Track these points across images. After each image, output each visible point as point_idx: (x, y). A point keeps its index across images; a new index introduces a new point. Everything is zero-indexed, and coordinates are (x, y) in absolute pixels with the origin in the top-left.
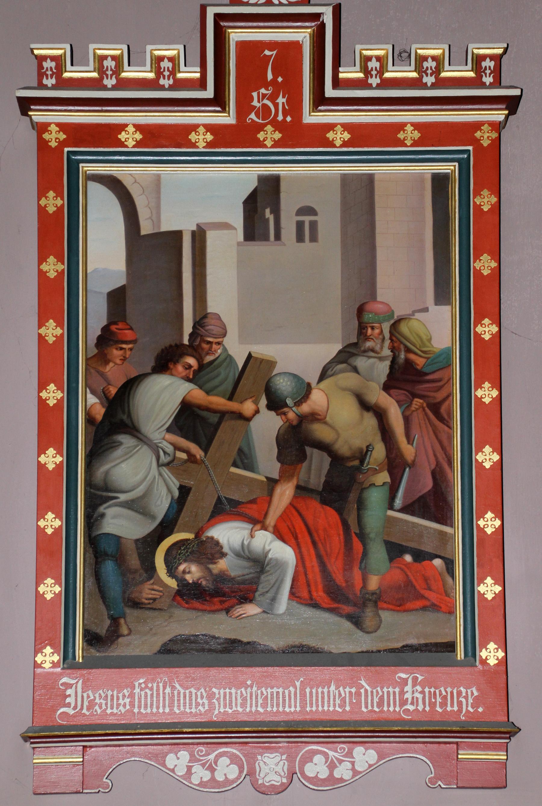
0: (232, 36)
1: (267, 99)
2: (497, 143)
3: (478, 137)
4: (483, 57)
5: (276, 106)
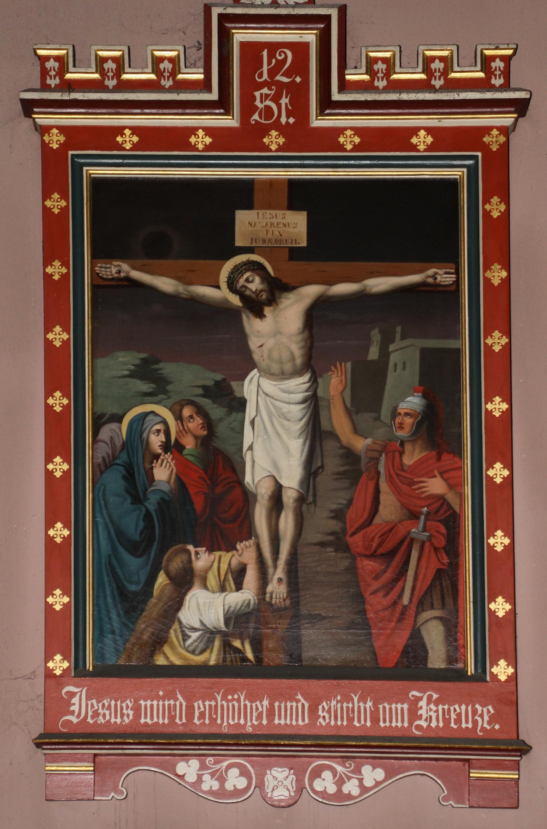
0: (236, 36)
1: (270, 100)
2: (505, 147)
3: (415, 142)
4: (433, 59)
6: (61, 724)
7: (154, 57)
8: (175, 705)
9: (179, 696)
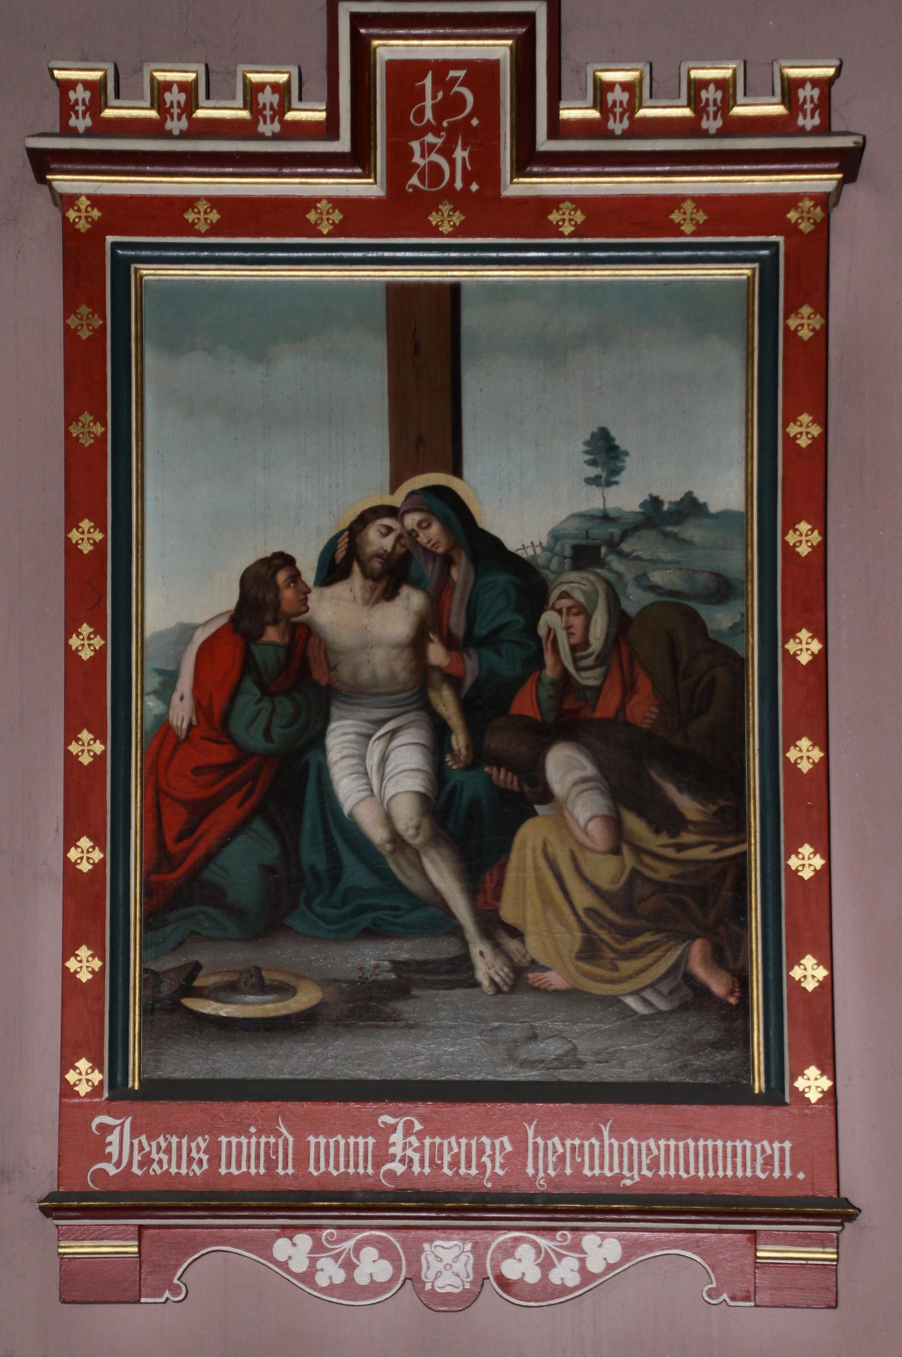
0: (379, 51)
2: (823, 227)
5: (452, 163)
6: (385, 1172)
7: (598, 82)
8: (276, 1144)
9: (283, 1129)
